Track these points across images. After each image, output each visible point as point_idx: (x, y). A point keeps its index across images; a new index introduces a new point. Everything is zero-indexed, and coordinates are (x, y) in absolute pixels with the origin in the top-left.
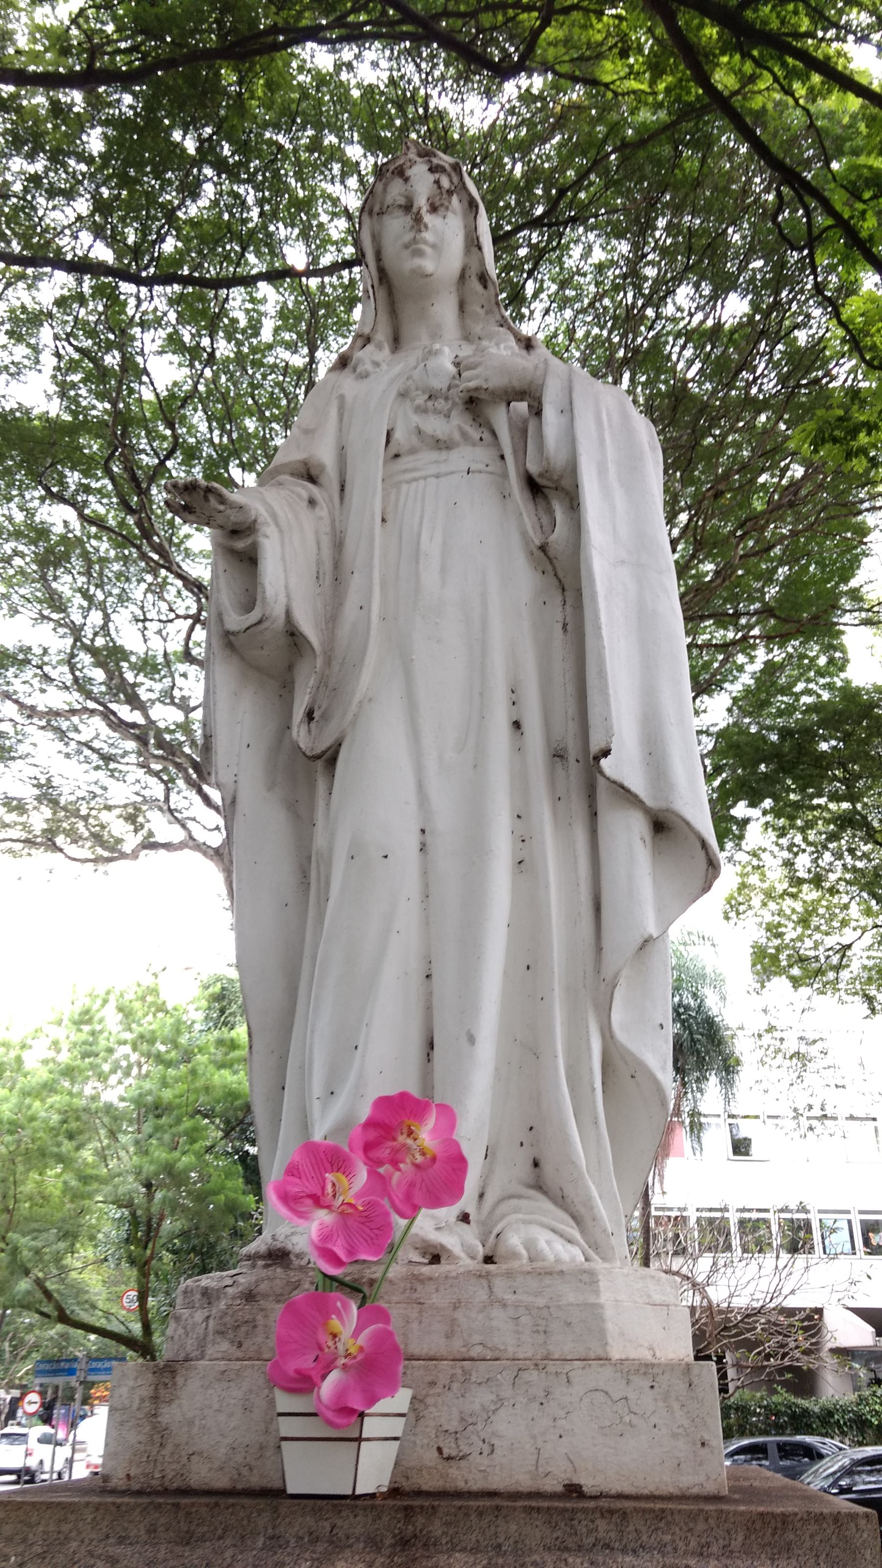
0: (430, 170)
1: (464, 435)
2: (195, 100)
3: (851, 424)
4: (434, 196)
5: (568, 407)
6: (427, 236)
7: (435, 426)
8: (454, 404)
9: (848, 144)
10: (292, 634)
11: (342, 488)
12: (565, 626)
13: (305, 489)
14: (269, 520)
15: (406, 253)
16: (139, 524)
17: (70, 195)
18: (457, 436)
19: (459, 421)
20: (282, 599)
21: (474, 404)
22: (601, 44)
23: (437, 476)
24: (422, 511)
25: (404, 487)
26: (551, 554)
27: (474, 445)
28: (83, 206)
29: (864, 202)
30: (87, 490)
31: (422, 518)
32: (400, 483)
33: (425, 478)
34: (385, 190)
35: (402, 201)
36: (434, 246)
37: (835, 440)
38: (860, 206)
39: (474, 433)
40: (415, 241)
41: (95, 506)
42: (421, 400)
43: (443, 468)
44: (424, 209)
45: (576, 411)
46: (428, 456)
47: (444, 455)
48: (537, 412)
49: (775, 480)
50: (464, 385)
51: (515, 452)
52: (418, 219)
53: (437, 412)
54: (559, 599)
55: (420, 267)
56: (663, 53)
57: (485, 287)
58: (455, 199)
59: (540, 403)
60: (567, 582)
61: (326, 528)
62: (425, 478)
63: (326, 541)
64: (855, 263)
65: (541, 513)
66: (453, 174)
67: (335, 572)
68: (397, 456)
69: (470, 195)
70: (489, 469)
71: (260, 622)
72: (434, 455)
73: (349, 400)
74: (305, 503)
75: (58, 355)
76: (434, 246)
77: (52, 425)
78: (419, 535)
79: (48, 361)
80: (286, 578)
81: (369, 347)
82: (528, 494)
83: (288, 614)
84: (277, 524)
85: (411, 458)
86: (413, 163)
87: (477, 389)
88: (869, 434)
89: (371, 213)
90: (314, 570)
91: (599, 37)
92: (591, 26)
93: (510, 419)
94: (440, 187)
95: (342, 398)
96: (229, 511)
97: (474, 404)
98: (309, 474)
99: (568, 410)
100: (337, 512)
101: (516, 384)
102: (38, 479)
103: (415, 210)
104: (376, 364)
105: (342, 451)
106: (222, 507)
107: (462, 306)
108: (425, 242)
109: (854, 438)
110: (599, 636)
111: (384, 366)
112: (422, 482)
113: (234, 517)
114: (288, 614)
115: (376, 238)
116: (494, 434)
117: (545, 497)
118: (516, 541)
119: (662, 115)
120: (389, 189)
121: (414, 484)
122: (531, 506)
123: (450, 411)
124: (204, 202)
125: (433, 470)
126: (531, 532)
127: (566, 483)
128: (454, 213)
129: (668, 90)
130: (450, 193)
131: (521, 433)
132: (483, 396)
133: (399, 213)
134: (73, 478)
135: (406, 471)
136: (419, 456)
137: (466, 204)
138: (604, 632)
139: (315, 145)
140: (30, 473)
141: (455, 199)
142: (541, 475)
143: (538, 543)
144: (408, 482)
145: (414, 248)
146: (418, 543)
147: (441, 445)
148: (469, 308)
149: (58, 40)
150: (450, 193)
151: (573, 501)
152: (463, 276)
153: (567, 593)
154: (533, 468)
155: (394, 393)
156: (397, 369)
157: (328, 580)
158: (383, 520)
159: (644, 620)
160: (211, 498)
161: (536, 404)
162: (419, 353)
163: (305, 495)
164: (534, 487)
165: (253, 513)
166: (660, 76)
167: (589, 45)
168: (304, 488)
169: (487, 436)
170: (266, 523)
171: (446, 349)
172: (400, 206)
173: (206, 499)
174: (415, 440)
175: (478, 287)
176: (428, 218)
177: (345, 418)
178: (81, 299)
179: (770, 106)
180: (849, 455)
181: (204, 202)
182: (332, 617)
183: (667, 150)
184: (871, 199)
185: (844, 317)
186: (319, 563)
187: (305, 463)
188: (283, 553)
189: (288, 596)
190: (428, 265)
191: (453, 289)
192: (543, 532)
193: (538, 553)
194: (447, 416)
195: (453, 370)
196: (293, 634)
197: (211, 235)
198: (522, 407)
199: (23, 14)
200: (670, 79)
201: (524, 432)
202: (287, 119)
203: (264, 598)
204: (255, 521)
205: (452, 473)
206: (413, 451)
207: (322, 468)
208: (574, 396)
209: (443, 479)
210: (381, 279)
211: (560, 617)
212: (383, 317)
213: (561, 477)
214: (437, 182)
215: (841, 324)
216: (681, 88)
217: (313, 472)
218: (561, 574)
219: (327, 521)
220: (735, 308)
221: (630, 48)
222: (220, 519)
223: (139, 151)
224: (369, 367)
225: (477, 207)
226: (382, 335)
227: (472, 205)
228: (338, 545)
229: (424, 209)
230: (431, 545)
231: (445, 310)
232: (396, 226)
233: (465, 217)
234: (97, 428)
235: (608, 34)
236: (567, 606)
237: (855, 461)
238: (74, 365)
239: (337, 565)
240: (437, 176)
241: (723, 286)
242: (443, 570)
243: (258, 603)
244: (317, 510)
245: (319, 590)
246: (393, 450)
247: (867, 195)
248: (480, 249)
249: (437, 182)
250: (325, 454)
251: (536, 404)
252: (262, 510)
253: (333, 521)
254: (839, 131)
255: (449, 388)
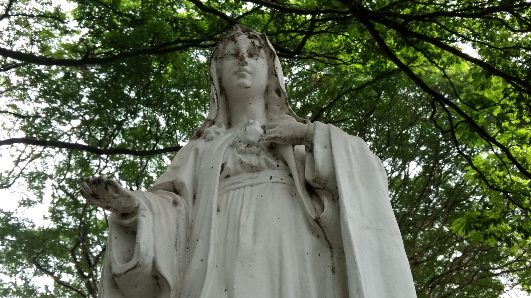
0: (249, 37)
1: (268, 164)
2: (138, 75)
3: (485, 220)
4: (251, 49)
5: (329, 145)
6: (247, 68)
7: (252, 160)
8: (262, 149)
9: (465, 88)
10: (156, 278)
11: (194, 197)
12: (333, 270)
13: (171, 196)
14: (147, 208)
15: (235, 77)
16: (88, 285)
17: (70, 117)
18: (263, 164)
19: (265, 157)
20: (151, 254)
21: (273, 148)
22: (337, 48)
23: (252, 186)
24: (242, 203)
25: (232, 193)
26: (322, 225)
27: (274, 169)
28: (76, 123)
29: (477, 110)
30: (61, 268)
31: (242, 207)
32: (229, 190)
33: (244, 187)
34: (224, 47)
35: (233, 52)
36: (250, 73)
37: (477, 228)
38: (475, 112)
39: (274, 163)
40: (240, 70)
41: (65, 278)
42: (243, 147)
43: (255, 181)
44: (246, 55)
45: (333, 146)
46: (246, 178)
47: (256, 175)
48: (310, 150)
49: (447, 259)
50: (267, 136)
51: (298, 171)
52: (242, 59)
53: (252, 153)
54: (329, 253)
55: (243, 83)
56: (368, 51)
57: (280, 96)
58: (262, 51)
59: (312, 145)
60: (333, 242)
61: (183, 216)
62: (244, 187)
63: (182, 224)
64: (476, 139)
65: (315, 203)
66: (261, 39)
67: (188, 240)
68: (228, 176)
69: (270, 49)
70: (283, 181)
71: (135, 267)
72: (250, 175)
73: (201, 151)
74: (171, 204)
75: (53, 196)
76: (250, 73)
77: (47, 233)
78: (240, 217)
79: (48, 199)
80: (155, 241)
81: (214, 126)
82: (306, 192)
83: (154, 263)
84: (151, 210)
85: (236, 177)
86: (239, 35)
87: (275, 138)
88: (495, 225)
89: (216, 59)
90: (174, 240)
91: (337, 45)
92: (333, 41)
93: (295, 155)
94: (254, 45)
95: (197, 150)
96: (120, 199)
97: (273, 148)
98: (175, 188)
99: (329, 146)
100: (190, 210)
101: (298, 134)
102: (33, 261)
103: (241, 54)
104: (218, 133)
105: (195, 182)
106: (116, 195)
107: (267, 107)
108: (246, 71)
109: (487, 227)
110: (355, 267)
111: (222, 134)
112: (242, 189)
113: (124, 203)
114: (154, 263)
115: (219, 71)
116: (286, 164)
117: (317, 195)
118: (300, 217)
119: (370, 77)
120: (226, 47)
121: (238, 190)
122: (308, 199)
123: (259, 152)
124: (138, 120)
125: (249, 182)
126: (309, 212)
127: (329, 185)
128: (262, 58)
129: (372, 67)
130: (259, 48)
131: (302, 162)
132: (279, 142)
133: (232, 58)
134: (53, 261)
135: (233, 184)
136: (240, 176)
137: (268, 53)
138: (359, 265)
139: (196, 95)
140: (28, 257)
141: (262, 51)
142: (314, 181)
143: (313, 217)
144: (234, 190)
145: (239, 74)
146: (239, 221)
147: (254, 169)
148: (270, 107)
149: (73, 49)
150: (259, 48)
151: (335, 196)
152: (267, 91)
153: (333, 250)
154: (309, 177)
155: (227, 145)
156: (230, 135)
157: (182, 246)
158: (218, 210)
159: (384, 262)
160: (110, 189)
161: (309, 145)
162: (242, 125)
163: (171, 199)
164: (311, 190)
165: (137, 202)
166: (367, 61)
167: (332, 48)
168: (171, 195)
169: (281, 164)
170: (145, 209)
171: (257, 122)
172: (232, 54)
173: (107, 189)
174: (238, 167)
175: (276, 96)
176: (247, 59)
177: (198, 160)
178: (69, 168)
179: (423, 73)
180: (486, 237)
181: (138, 120)
182: (183, 270)
183: (374, 93)
184: (480, 109)
185: (475, 165)
186: (177, 236)
187: (172, 183)
188: (154, 227)
189: (155, 252)
190: (247, 82)
191: (262, 96)
192: (316, 212)
193: (314, 224)
194: (258, 155)
195: (261, 131)
196: (157, 277)
197: (140, 134)
198: (301, 148)
199: (56, 39)
200: (373, 62)
201: (303, 163)
202: (183, 83)
203: (139, 252)
204: (137, 208)
205: (261, 183)
206: (237, 173)
207: (183, 185)
208: (332, 138)
209: (255, 188)
210: (221, 93)
211: (330, 264)
212: (222, 112)
213: (326, 181)
214: (253, 43)
215: (474, 168)
216: (378, 66)
217: (177, 188)
218: (329, 238)
219: (184, 212)
220: (414, 169)
221: (352, 49)
222: (114, 204)
223: (108, 99)
224: (213, 135)
225: (274, 55)
226: (222, 119)
227: (272, 54)
228: (190, 228)
229: (246, 55)
230: (247, 222)
231: (257, 107)
232: (230, 64)
233: (268, 60)
234: (69, 234)
235: (341, 44)
236: (334, 258)
237: (490, 240)
238: (62, 201)
239: (188, 240)
240: (253, 40)
241: (407, 159)
242: (255, 234)
243: (135, 255)
244: (178, 208)
245: (176, 253)
246: (225, 173)
247: (478, 107)
248: (276, 76)
249: (253, 43)
250: (185, 178)
251: (309, 145)
252: (142, 202)
253: (187, 215)
254: (459, 83)
255: (259, 141)
